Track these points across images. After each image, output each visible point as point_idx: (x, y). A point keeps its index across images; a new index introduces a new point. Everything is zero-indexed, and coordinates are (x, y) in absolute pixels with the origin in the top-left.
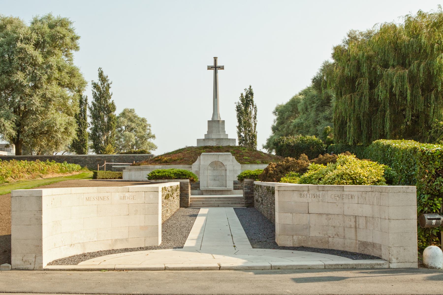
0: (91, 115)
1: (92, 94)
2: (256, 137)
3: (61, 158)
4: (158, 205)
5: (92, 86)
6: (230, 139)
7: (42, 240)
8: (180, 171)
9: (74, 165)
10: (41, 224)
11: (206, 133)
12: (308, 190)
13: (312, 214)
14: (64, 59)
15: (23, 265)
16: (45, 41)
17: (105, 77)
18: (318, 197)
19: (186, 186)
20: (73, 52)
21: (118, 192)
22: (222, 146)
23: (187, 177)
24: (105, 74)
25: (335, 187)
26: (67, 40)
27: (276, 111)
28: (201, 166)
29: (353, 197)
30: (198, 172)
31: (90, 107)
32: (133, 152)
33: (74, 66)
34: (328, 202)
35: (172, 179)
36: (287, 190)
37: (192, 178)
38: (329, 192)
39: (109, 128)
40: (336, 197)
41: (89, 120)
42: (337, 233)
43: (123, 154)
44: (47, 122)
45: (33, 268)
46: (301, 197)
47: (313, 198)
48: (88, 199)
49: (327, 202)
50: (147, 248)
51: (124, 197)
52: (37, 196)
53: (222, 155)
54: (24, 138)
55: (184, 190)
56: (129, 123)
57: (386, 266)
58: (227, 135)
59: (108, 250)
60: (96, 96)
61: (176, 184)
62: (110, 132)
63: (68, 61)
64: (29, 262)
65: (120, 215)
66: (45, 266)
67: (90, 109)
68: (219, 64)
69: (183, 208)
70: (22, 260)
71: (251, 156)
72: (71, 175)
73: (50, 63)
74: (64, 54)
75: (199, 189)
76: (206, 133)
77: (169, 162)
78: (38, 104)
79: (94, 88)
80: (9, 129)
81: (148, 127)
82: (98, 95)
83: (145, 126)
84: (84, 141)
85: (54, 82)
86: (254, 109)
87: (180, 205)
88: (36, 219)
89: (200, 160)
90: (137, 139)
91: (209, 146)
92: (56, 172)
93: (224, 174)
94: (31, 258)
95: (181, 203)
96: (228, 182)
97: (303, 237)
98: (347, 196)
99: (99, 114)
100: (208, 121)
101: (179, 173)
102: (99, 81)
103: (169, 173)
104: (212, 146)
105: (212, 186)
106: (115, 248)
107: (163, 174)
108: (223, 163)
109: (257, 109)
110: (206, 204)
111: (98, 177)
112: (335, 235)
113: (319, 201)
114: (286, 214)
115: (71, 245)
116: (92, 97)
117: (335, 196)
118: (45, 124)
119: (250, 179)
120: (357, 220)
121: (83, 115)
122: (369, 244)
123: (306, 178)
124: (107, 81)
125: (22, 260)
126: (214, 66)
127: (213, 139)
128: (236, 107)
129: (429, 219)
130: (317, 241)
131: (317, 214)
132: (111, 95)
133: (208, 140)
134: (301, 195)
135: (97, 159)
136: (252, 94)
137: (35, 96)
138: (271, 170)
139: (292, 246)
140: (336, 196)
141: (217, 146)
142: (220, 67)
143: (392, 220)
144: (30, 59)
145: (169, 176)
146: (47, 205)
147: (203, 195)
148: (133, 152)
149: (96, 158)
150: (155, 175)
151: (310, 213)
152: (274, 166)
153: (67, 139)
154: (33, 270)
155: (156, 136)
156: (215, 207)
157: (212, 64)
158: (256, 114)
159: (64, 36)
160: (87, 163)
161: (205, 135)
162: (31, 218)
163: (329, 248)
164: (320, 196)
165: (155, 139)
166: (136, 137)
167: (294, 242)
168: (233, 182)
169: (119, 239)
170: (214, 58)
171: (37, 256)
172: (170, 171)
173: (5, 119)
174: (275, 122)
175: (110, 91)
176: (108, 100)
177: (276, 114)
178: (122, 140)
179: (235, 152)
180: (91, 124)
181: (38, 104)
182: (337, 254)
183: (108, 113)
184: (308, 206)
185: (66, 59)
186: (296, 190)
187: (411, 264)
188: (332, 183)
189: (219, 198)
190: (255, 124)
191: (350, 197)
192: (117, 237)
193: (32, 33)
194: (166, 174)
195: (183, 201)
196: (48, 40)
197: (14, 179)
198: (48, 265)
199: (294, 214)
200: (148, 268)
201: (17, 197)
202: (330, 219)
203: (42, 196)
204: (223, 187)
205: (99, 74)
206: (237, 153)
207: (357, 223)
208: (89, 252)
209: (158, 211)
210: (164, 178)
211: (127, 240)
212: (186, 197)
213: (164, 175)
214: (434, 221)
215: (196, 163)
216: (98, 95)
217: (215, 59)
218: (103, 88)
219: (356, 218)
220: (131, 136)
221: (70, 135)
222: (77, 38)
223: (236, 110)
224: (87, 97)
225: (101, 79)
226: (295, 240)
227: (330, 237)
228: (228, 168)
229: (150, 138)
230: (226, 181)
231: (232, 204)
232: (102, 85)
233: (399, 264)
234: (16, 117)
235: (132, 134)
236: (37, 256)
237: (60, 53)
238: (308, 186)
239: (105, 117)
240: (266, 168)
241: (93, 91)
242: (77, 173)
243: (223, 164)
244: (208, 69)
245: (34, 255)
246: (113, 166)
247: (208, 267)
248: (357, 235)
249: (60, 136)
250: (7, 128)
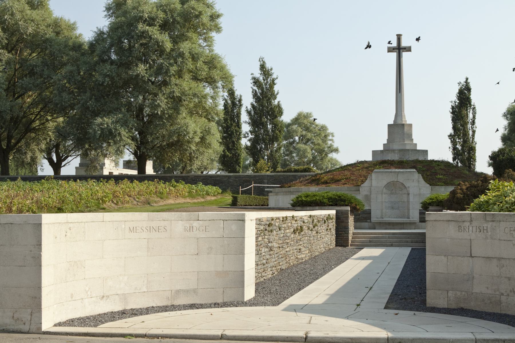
0: (250, 121)
1: (251, 92)
2: (475, 150)
3: (196, 177)
4: (244, 240)
5: (252, 81)
7: (41, 289)
8: (337, 195)
9: (210, 187)
10: (39, 265)
11: (386, 142)
12: (471, 221)
13: (477, 258)
14: (202, 44)
15: (13, 325)
16: (174, 20)
17: (268, 70)
18: (485, 231)
19: (345, 216)
20: (213, 34)
21: (181, 220)
22: (407, 161)
23: (347, 203)
24: (268, 66)
25: (510, 216)
26: (205, 19)
27: (508, 114)
28: (372, 188)
30: (368, 198)
31: (249, 110)
32: (293, 170)
33: (216, 54)
34: (501, 239)
35: (325, 206)
36: (439, 221)
37: (353, 205)
38: (502, 223)
39: (274, 139)
40: (511, 232)
41: (246, 128)
42: (513, 289)
43: (280, 172)
44: (176, 130)
45: (28, 330)
46: (460, 230)
47: (477, 233)
48: (132, 230)
49: (499, 240)
50: (225, 305)
51: (191, 228)
52: (34, 224)
53: (403, 172)
54: (147, 151)
55: (343, 222)
56: (304, 133)
58: (416, 144)
59: (164, 306)
60: (257, 94)
62: (276, 144)
63: (206, 47)
64: (22, 321)
65: (185, 255)
66: (45, 327)
67: (249, 113)
68: (404, 44)
69: (340, 248)
70: (13, 317)
71: (447, 175)
72: (203, 200)
73: (181, 50)
74: (202, 37)
75: (371, 220)
76: (386, 142)
77: (329, 183)
78: (163, 105)
79: (253, 85)
80: (127, 139)
81: (330, 138)
82: (259, 95)
83: (326, 136)
84: (238, 156)
85: (187, 76)
86: (472, 110)
87: (336, 241)
88: (33, 257)
89: (371, 179)
90: (315, 154)
91: (388, 160)
92: (182, 197)
93: (406, 200)
94: (25, 316)
95: (338, 240)
96: (411, 211)
97: (463, 293)
99: (261, 120)
100: (388, 125)
101: (335, 198)
102: (260, 75)
103: (321, 198)
104: (393, 161)
105: (389, 217)
106: (177, 303)
107: (312, 199)
108: (404, 184)
109: (477, 111)
110: (374, 241)
111: (238, 203)
112: (511, 291)
113: (486, 238)
114: (438, 256)
115: (103, 297)
116: (252, 96)
117: (510, 231)
118: (174, 132)
119: (438, 207)
121: (236, 120)
123: (481, 203)
124: (271, 75)
125: (13, 317)
126: (398, 48)
127: (395, 150)
128: (451, 107)
130: (483, 300)
131: (484, 257)
132: (277, 94)
133: (387, 152)
134: (460, 227)
135: (244, 179)
136: (469, 89)
137: (160, 95)
138: (460, 193)
139: (447, 307)
141: (400, 160)
144: (155, 45)
145: (321, 202)
146: (56, 237)
147: (375, 229)
148: (293, 170)
149: (243, 178)
150: (302, 201)
151: (473, 255)
152: (464, 187)
153: (204, 152)
154: (28, 333)
155: (340, 149)
156: (387, 246)
158: (474, 117)
159: (200, 13)
160: (231, 185)
161: (384, 145)
162: (25, 256)
163: (502, 313)
164: (489, 230)
165: (339, 154)
166: (313, 151)
167: (450, 300)
168: (418, 211)
169: (182, 290)
170: (397, 35)
171: (34, 313)
172: (323, 195)
173: (122, 126)
174: (506, 130)
175: (276, 88)
176: (273, 101)
177: (508, 118)
178: (294, 155)
179: (424, 169)
180: (250, 134)
181: (163, 105)
183: (273, 119)
184: (470, 245)
185: (205, 44)
186: (452, 221)
188: (510, 209)
189: (394, 234)
190: (474, 132)
192: (179, 288)
193: (158, 10)
194: (316, 199)
195: (341, 238)
196: (178, 19)
197: (116, 204)
198: (55, 325)
199: (450, 257)
200: (207, 336)
201: (7, 225)
202: (503, 266)
203: (41, 224)
204: (405, 218)
205: (260, 65)
206: (427, 170)
208: (134, 308)
209: (244, 249)
210: (313, 205)
211: (195, 291)
212: (344, 231)
213: (313, 200)
215: (366, 184)
216: (259, 95)
217: (399, 37)
218: (266, 85)
220: (306, 149)
221: (209, 146)
222: (218, 16)
223: (451, 111)
224: (241, 96)
225: (262, 73)
226: (451, 299)
227: (502, 294)
228: (411, 191)
229: (332, 152)
230: (409, 210)
231: (412, 242)
232: (264, 80)
234: (136, 122)
235: (308, 148)
236: (34, 313)
237: (194, 36)
238: (471, 213)
239: (268, 123)
240: (453, 190)
241: (252, 89)
242: (213, 198)
243: (405, 186)
244: (388, 52)
245: (29, 311)
246: (266, 190)
247: (287, 338)
249: (194, 148)
250: (124, 138)
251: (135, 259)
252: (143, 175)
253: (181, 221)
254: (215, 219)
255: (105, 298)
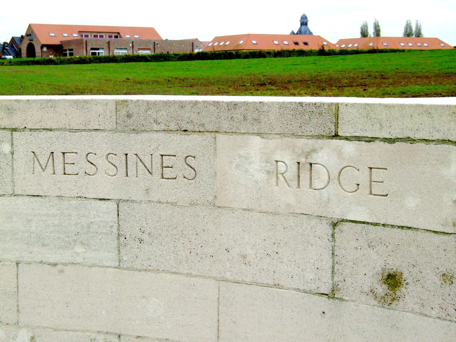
21: (259, 134)
251: (62, 271)
253: (257, 139)
254: (418, 136)
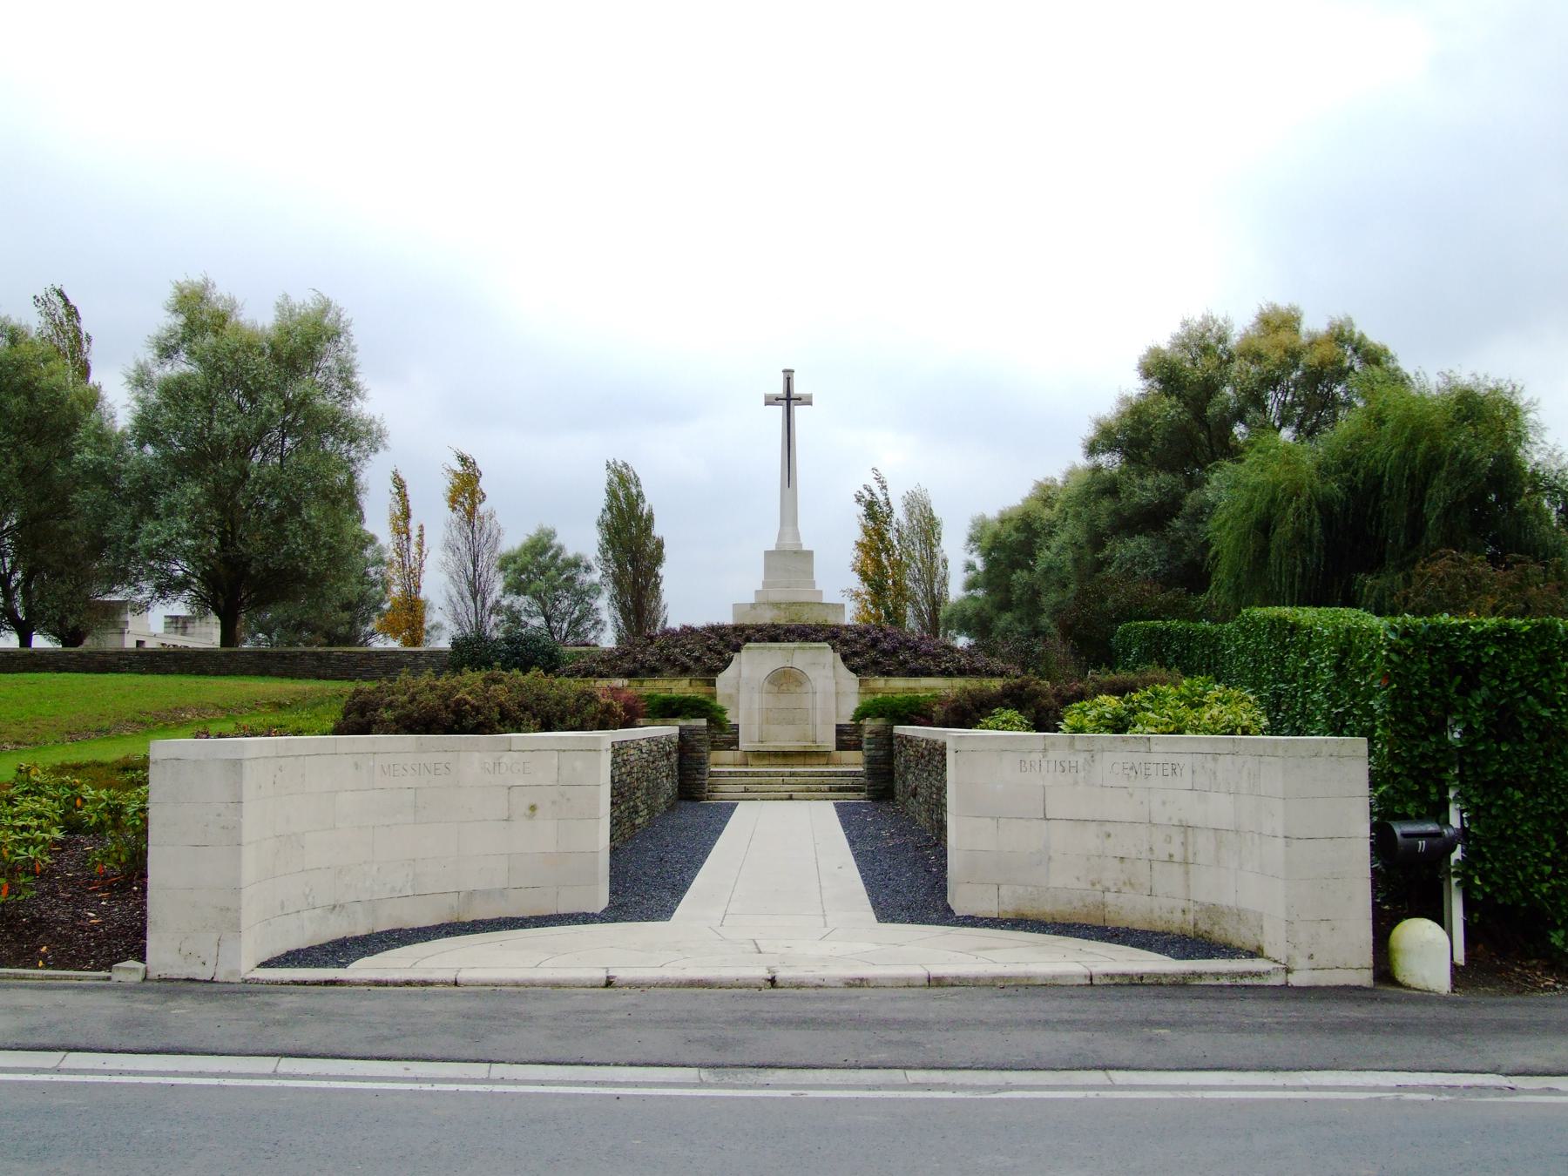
6: (827, 605)
11: (760, 587)
18: (1073, 770)
21: (478, 751)
29: (1178, 770)
38: (1106, 754)
40: (1126, 772)
45: (1402, 975)
46: (1024, 769)
57: (1277, 980)
61: (667, 731)
76: (760, 587)
97: (1030, 889)
98: (1160, 767)
112: (1125, 883)
113: (1076, 783)
115: (335, 907)
120: (1191, 839)
122: (1226, 911)
129: (1405, 835)
140: (1127, 766)
142: (800, 399)
143: (1294, 841)
157: (779, 390)
182: (986, 925)
187: (63, 1066)
191: (1169, 771)
198: (265, 965)
207: (1190, 849)
214: (1422, 844)
217: (788, 376)
219: (1185, 833)
227: (1108, 890)
233: (1316, 973)
244: (767, 404)
245: (215, 937)
248: (1188, 886)
252: (29, 650)
255: (337, 909)
